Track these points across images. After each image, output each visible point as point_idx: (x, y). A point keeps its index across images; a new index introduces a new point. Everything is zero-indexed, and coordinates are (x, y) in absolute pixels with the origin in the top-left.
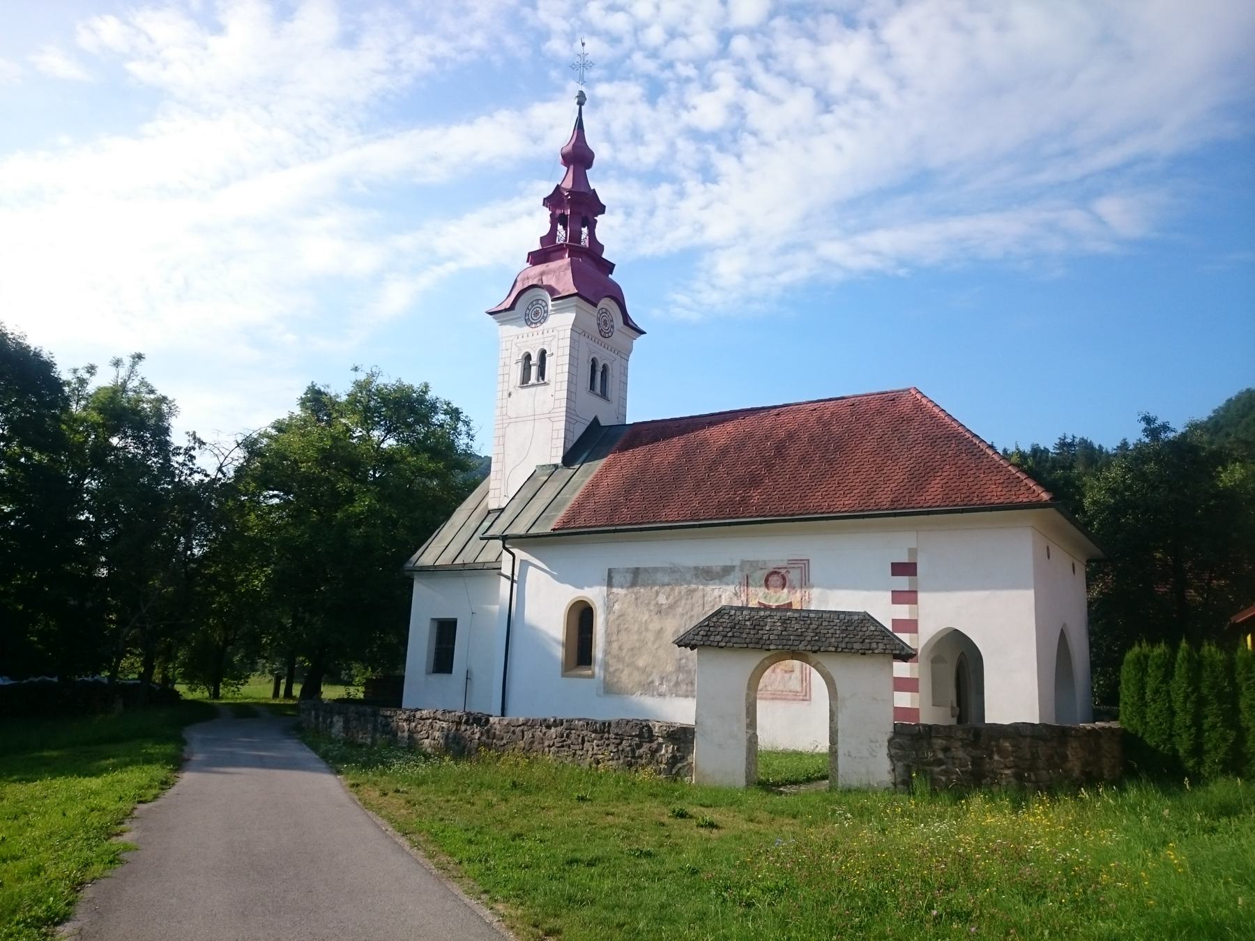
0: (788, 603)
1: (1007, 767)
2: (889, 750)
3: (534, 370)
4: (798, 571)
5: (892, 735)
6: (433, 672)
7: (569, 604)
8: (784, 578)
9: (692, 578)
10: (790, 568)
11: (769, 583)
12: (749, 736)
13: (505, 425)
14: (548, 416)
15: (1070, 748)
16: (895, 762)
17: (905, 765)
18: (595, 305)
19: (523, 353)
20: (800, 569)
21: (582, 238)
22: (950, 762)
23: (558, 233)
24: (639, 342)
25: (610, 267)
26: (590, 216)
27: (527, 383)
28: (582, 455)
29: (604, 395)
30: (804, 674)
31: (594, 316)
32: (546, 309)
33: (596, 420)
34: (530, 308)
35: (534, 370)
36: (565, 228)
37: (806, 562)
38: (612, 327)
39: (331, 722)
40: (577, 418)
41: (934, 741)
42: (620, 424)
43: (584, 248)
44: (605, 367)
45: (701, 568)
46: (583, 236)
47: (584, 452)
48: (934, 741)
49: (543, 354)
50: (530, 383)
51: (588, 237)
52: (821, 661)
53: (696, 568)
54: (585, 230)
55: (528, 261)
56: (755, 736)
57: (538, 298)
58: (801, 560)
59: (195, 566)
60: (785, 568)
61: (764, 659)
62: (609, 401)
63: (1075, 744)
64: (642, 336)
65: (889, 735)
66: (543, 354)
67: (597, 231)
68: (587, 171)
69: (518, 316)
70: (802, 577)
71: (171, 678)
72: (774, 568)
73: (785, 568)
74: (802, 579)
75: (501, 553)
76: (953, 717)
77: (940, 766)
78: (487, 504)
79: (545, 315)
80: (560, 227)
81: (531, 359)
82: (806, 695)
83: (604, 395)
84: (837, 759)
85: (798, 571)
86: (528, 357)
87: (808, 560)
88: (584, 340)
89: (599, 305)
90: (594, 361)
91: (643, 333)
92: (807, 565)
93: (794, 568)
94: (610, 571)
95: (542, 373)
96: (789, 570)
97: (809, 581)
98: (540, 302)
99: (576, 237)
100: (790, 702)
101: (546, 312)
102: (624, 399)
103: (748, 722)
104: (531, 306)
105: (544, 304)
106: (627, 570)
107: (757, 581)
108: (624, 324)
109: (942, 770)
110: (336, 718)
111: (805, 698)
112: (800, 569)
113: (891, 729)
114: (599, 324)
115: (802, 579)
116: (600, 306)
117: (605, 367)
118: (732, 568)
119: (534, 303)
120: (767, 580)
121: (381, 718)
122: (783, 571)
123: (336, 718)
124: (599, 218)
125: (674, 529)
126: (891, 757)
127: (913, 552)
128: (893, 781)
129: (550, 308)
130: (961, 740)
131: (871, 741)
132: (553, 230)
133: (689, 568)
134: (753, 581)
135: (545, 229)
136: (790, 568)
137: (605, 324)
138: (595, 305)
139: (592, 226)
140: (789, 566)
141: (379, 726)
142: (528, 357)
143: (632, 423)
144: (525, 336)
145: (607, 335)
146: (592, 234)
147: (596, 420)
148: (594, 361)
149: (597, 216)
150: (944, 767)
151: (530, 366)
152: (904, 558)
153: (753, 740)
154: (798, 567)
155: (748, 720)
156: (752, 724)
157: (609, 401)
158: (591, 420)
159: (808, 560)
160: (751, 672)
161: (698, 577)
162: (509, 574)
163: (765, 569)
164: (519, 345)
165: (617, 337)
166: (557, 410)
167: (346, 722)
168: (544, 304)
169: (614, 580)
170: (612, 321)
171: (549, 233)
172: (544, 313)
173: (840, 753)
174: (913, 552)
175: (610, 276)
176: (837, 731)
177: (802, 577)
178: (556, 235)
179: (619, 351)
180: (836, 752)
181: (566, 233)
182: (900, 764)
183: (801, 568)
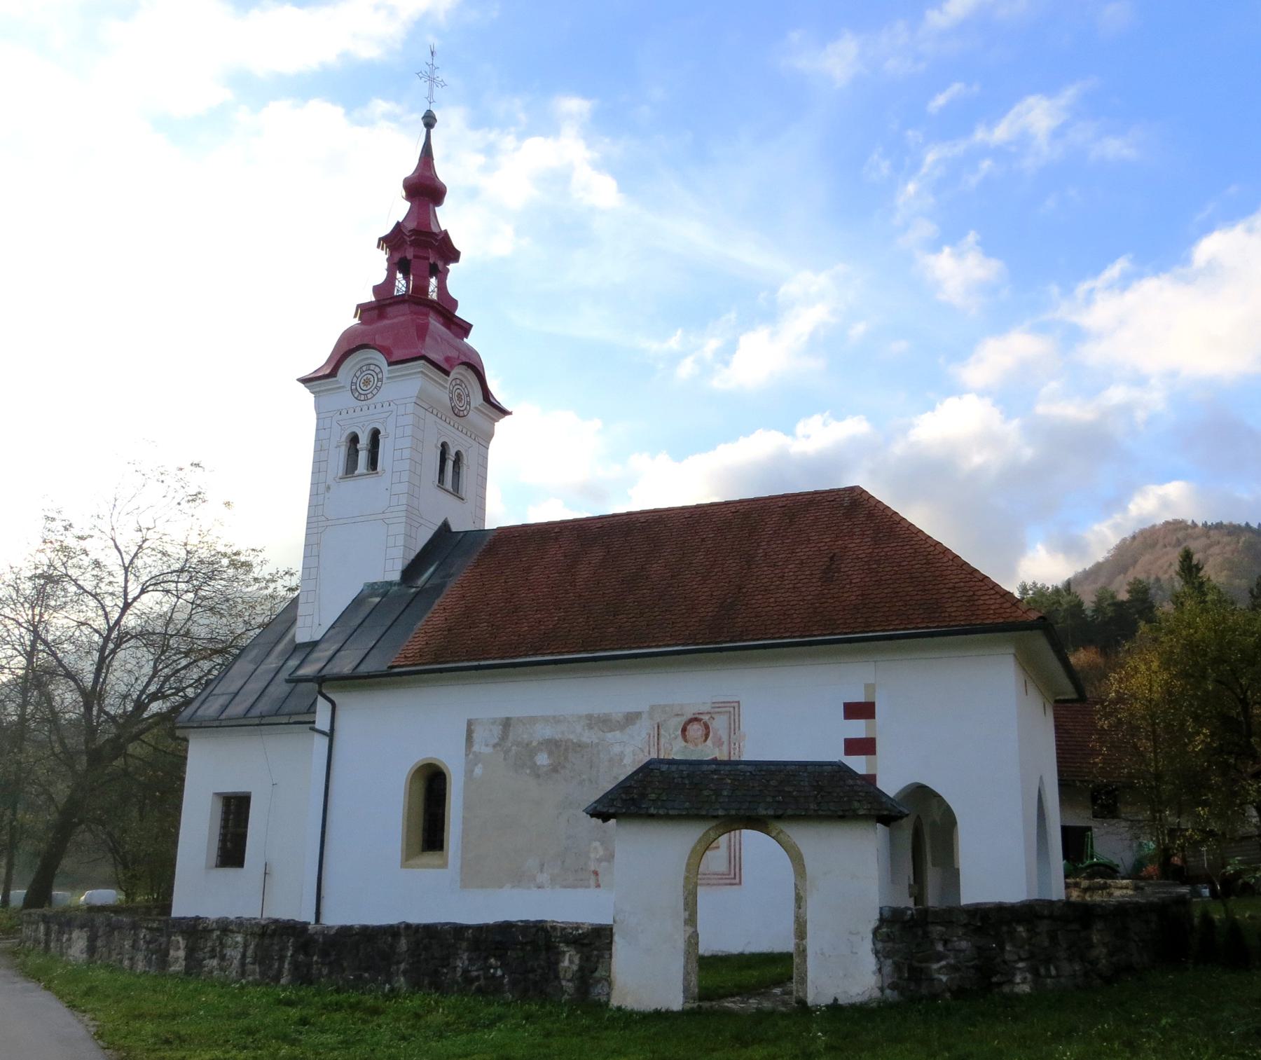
1: (1021, 960)
2: (874, 944)
3: (363, 457)
4: (725, 717)
5: (878, 923)
6: (216, 866)
7: (416, 764)
8: (707, 727)
9: (584, 730)
11: (687, 733)
12: (688, 935)
13: (320, 530)
14: (381, 516)
15: (1095, 931)
16: (882, 959)
17: (894, 963)
18: (447, 373)
19: (370, 428)
21: (430, 290)
22: (952, 956)
23: (397, 282)
24: (501, 426)
25: (465, 328)
26: (440, 264)
27: (353, 473)
28: (426, 570)
29: (456, 491)
30: (733, 850)
31: (445, 388)
32: (380, 376)
33: (445, 526)
34: (354, 381)
35: (363, 457)
36: (406, 277)
37: (736, 705)
38: (469, 403)
39: (69, 939)
40: (422, 521)
41: (931, 928)
42: (476, 529)
43: (432, 301)
44: (458, 454)
46: (431, 289)
47: (432, 565)
48: (931, 928)
49: (375, 435)
50: (356, 472)
51: (436, 289)
52: (782, 828)
53: (589, 717)
54: (433, 281)
55: (355, 317)
56: (695, 935)
57: (369, 361)
59: (1105, 704)
61: (710, 829)
62: (463, 499)
63: (1099, 925)
64: (507, 417)
65: (874, 923)
66: (375, 435)
67: (448, 282)
68: (437, 209)
69: (341, 385)
72: (694, 714)
74: (730, 728)
75: (317, 698)
76: (910, 897)
77: (939, 961)
78: (294, 636)
79: (379, 384)
80: (399, 276)
81: (358, 442)
82: (735, 878)
83: (456, 491)
84: (805, 961)
85: (725, 717)
86: (354, 439)
87: (739, 702)
88: (430, 418)
89: (452, 374)
90: (444, 445)
91: (504, 412)
92: (736, 709)
93: (718, 713)
94: (470, 724)
95: (373, 463)
96: (713, 716)
98: (372, 367)
99: (421, 289)
100: (714, 887)
101: (380, 380)
102: (482, 498)
103: (687, 917)
104: (359, 372)
105: (377, 370)
106: (494, 722)
107: (671, 732)
108: (484, 400)
109: (941, 968)
110: (75, 934)
111: (733, 881)
113: (877, 916)
114: (451, 399)
116: (453, 375)
117: (458, 454)
118: (638, 715)
119: (364, 368)
120: (684, 730)
121: (144, 930)
122: (705, 718)
123: (75, 934)
124: (451, 267)
125: (639, 657)
126: (876, 953)
127: (870, 688)
128: (880, 985)
129: (386, 375)
130: (965, 926)
131: (851, 933)
132: (390, 279)
133: (580, 717)
134: (665, 731)
135: (380, 276)
137: (459, 396)
138: (447, 373)
139: (442, 275)
140: (713, 710)
141: (142, 942)
142: (354, 439)
143: (495, 528)
144: (379, 406)
145: (461, 414)
146: (442, 287)
147: (445, 526)
148: (444, 445)
149: (449, 265)
150: (943, 963)
151: (357, 451)
152: (859, 697)
153: (693, 941)
154: (726, 712)
155: (687, 913)
156: (691, 920)
157: (463, 499)
158: (439, 524)
159: (739, 702)
161: (592, 728)
162: (327, 728)
163: (682, 715)
164: (341, 423)
165: (473, 416)
166: (392, 509)
167: (92, 940)
168: (377, 370)
169: (475, 735)
170: (468, 395)
171: (454, 248)
172: (378, 381)
173: (809, 952)
174: (870, 688)
175: (465, 340)
176: (805, 922)
178: (394, 285)
179: (476, 436)
180: (804, 950)
181: (408, 283)
182: (889, 962)
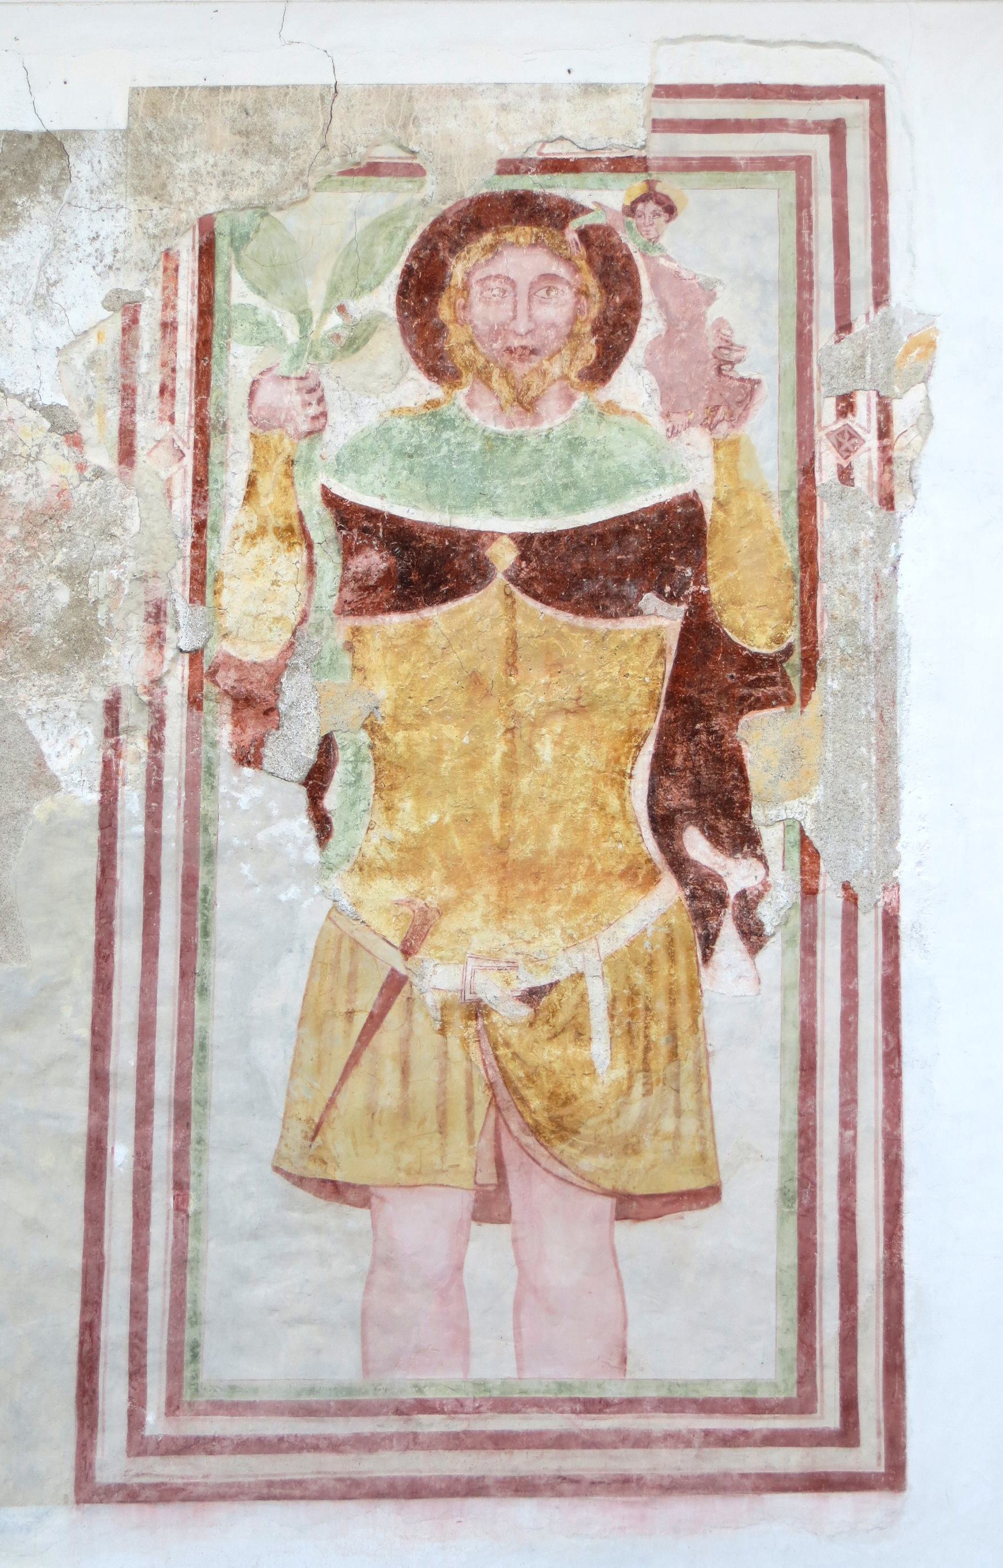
0: (664, 511)
10: (686, 165)
20: (789, 179)
45: (635, 1477)
58: (798, 93)
60: (621, 165)
70: (804, 255)
71: (102, 624)
72: (509, 167)
73: (621, 165)
74: (805, 284)
87: (875, 95)
96: (668, 185)
97: (880, 296)
107: (316, 295)
112: (789, 179)
115: (805, 284)
136: (686, 165)
140: (661, 146)
154: (773, 164)
159: (875, 95)
160: (351, 1208)
163: (413, 171)
177: (804, 255)
183: (802, 164)
